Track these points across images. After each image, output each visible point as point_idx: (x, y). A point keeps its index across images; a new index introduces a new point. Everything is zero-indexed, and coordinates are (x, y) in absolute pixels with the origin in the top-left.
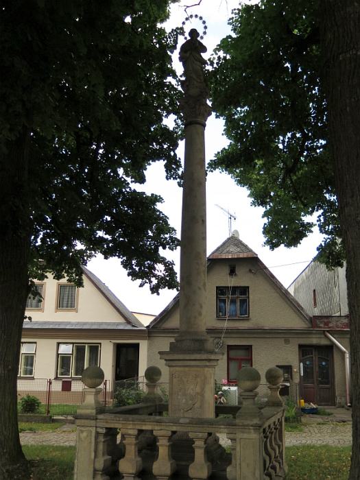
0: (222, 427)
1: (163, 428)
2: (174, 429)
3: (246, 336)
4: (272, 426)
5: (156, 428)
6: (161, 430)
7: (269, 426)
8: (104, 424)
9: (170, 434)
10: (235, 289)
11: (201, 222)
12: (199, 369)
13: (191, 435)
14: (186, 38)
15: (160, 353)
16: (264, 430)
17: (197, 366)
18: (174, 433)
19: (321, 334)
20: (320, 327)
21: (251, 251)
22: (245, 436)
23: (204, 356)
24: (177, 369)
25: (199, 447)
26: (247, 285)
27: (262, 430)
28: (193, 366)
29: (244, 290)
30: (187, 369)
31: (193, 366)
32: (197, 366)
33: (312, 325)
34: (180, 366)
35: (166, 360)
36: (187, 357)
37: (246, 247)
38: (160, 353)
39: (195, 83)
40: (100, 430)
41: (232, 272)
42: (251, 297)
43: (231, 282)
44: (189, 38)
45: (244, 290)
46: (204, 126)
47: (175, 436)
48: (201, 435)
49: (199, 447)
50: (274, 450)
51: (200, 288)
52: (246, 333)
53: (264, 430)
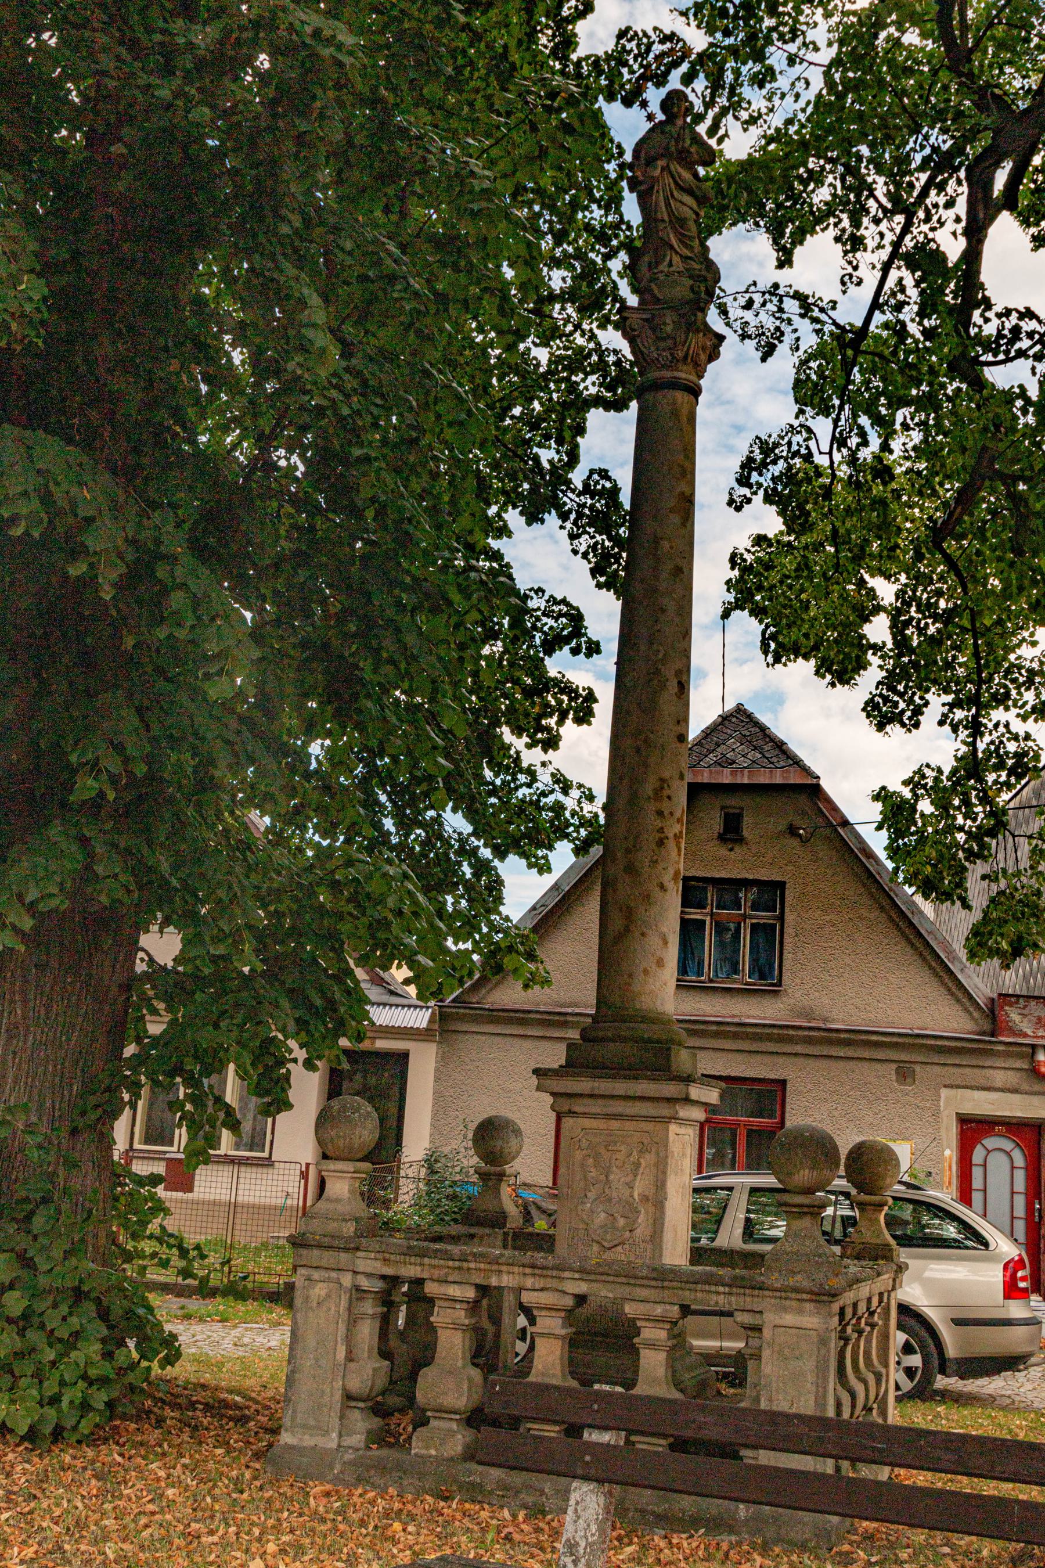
0: (721, 1289)
1: (550, 1283)
2: (582, 1288)
3: (771, 1047)
4: (862, 1308)
5: (529, 1282)
6: (542, 1290)
7: (855, 1305)
8: (378, 1264)
9: (569, 1302)
10: (730, 888)
11: (673, 687)
12: (650, 1127)
13: (629, 1309)
14: (650, 117)
15: (537, 1072)
16: (842, 1310)
17: (647, 1118)
18: (581, 1299)
19: (1021, 1056)
20: (1026, 1035)
21: (797, 762)
22: (789, 1319)
23: (670, 1089)
24: (587, 1123)
25: (652, 1345)
26: (777, 877)
27: (836, 1307)
28: (632, 1118)
29: (772, 893)
30: (615, 1124)
31: (632, 1118)
32: (647, 1118)
33: (555, 1182)
34: (594, 1116)
35: (553, 1094)
36: (620, 1087)
37: (780, 746)
38: (537, 1072)
39: (676, 259)
40: (364, 1283)
41: (731, 832)
42: (790, 917)
43: (731, 865)
44: (660, 117)
45: (772, 893)
46: (695, 392)
47: (583, 1311)
48: (659, 1310)
49: (652, 1345)
50: (864, 1382)
51: (662, 887)
52: (770, 1038)
53: (842, 1310)
